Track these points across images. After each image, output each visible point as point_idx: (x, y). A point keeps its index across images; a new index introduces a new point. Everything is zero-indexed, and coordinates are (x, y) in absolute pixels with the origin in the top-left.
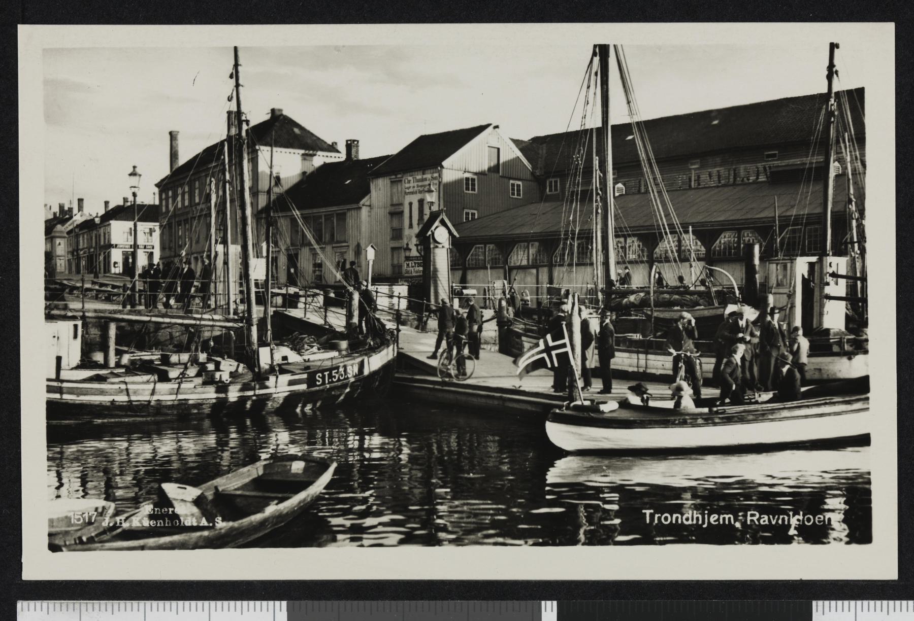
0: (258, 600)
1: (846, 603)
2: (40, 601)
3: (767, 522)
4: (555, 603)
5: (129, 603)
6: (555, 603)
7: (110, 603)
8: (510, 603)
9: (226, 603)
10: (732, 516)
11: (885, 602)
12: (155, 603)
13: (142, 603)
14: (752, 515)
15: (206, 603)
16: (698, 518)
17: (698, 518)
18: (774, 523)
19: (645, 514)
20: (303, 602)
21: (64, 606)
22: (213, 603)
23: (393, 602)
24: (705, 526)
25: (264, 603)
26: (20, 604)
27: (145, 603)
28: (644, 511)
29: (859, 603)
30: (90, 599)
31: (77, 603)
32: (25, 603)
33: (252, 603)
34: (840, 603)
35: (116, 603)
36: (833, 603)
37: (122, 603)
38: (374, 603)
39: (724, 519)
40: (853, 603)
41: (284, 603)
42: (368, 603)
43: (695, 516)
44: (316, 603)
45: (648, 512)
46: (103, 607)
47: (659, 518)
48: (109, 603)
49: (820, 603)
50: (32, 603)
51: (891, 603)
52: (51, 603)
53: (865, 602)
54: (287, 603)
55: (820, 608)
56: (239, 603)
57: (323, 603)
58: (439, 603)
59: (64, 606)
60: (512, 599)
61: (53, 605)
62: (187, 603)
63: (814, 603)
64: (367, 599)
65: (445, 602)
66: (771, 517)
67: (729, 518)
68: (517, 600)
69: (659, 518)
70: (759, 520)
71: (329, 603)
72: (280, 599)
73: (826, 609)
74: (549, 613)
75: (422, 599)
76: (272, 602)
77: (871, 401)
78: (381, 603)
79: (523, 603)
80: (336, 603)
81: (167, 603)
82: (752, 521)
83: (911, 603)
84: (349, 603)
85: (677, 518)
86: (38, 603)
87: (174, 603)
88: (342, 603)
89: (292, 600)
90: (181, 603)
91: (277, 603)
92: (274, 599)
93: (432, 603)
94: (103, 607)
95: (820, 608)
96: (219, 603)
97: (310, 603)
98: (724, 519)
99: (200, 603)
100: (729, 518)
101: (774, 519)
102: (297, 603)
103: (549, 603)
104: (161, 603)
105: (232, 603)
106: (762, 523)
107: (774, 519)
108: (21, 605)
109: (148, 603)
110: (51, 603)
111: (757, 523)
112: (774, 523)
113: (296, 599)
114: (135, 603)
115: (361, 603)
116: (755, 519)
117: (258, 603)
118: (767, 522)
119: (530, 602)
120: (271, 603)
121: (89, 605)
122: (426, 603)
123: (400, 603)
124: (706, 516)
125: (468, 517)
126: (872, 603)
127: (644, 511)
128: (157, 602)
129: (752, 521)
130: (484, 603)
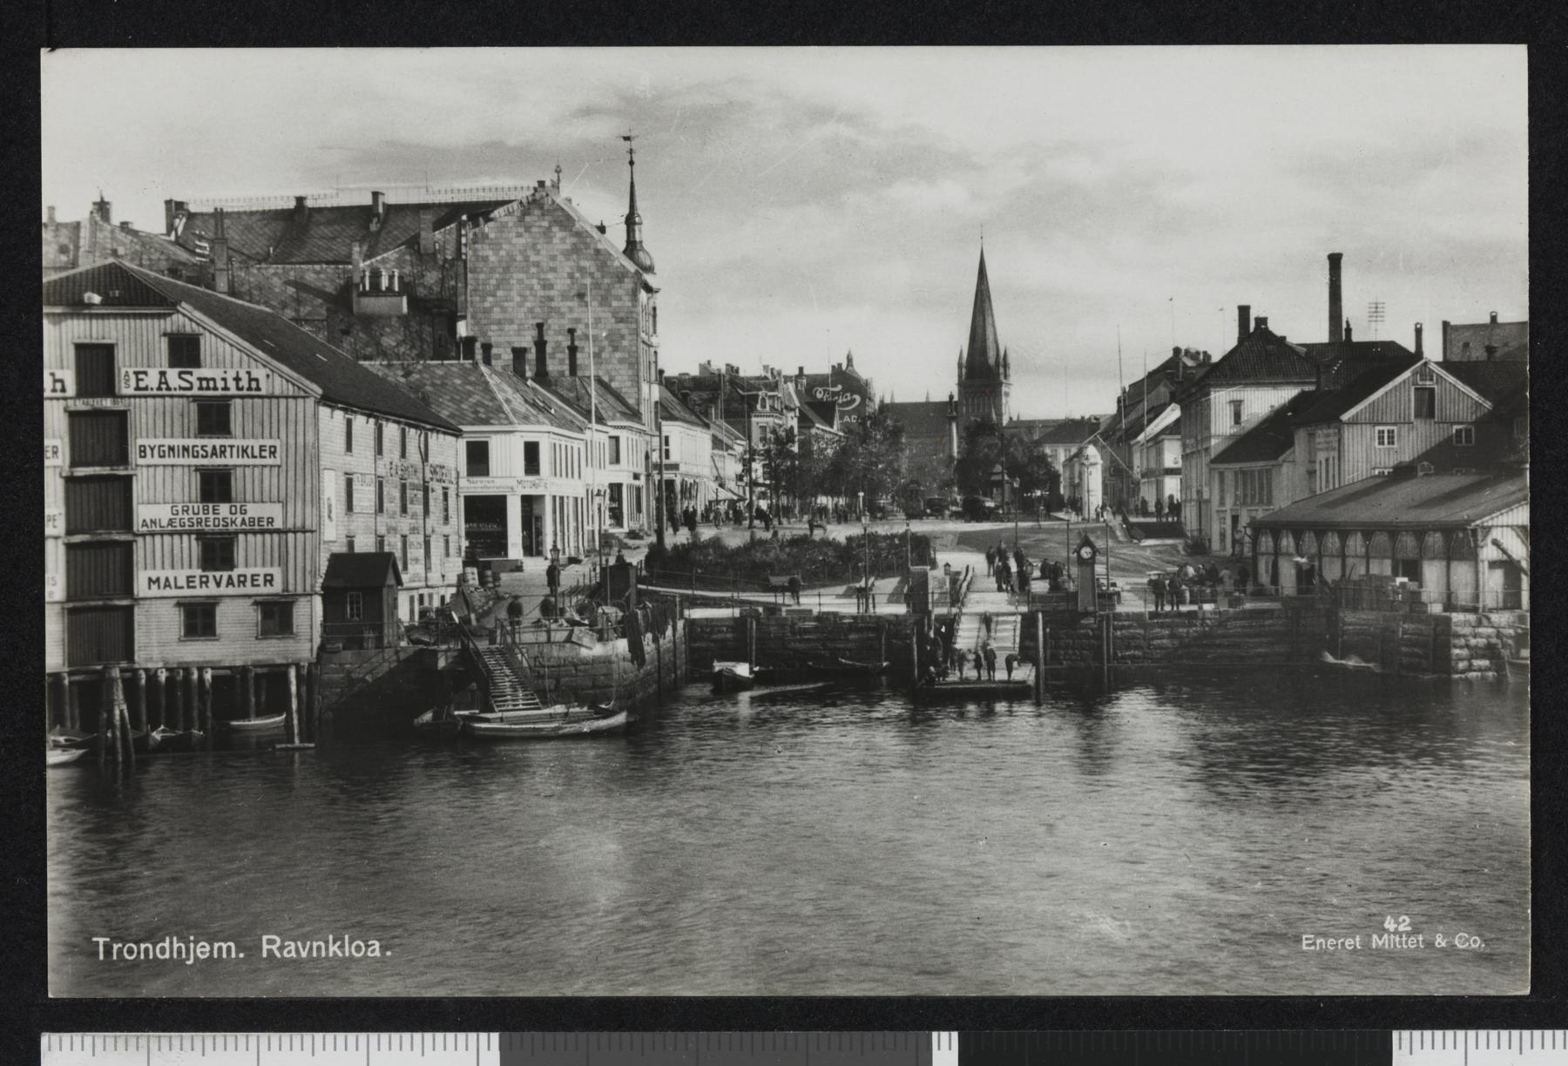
0: (450, 1031)
1: (1450, 1033)
2: (80, 1034)
3: (293, 954)
4: (955, 1035)
5: (230, 1036)
6: (955, 1035)
7: (198, 1036)
8: (878, 1035)
9: (395, 1036)
10: (232, 944)
11: (1515, 1033)
12: (275, 1036)
13: (253, 1036)
14: (271, 942)
15: (363, 1036)
16: (179, 952)
17: (179, 949)
18: (304, 954)
19: (98, 942)
20: (527, 1035)
21: (121, 1042)
22: (373, 1036)
23: (680, 1035)
24: (188, 963)
25: (461, 1036)
26: (46, 1039)
27: (182, 1037)
28: (95, 939)
29: (1471, 1033)
30: (164, 1031)
31: (143, 1037)
32: (55, 1037)
33: (439, 1036)
34: (1439, 1034)
35: (209, 1036)
36: (1428, 1034)
37: (220, 1036)
38: (648, 1035)
39: (220, 949)
40: (1461, 1034)
41: (495, 1036)
42: (637, 1035)
43: (176, 946)
44: (549, 1036)
45: (101, 940)
46: (187, 1043)
47: (120, 951)
48: (198, 1037)
49: (1406, 1034)
50: (66, 1037)
51: (1526, 1033)
52: (99, 1036)
53: (1482, 1033)
54: (500, 1037)
55: (1406, 1043)
56: (417, 1036)
57: (560, 1035)
58: (758, 1035)
59: (121, 1042)
60: (881, 1029)
61: (244, 1039)
62: (330, 1036)
63: (1395, 1034)
64: (636, 1030)
65: (769, 1034)
66: (299, 944)
67: (229, 949)
68: (891, 1029)
69: (120, 951)
70: (281, 949)
71: (571, 1035)
72: (488, 1028)
73: (1416, 1045)
74: (945, 1052)
75: (729, 1029)
76: (475, 1034)
77: (565, 495)
78: (658, 1035)
79: (901, 1035)
80: (583, 1035)
81: (297, 1036)
82: (270, 952)
83: (1559, 1033)
84: (604, 1035)
85: (147, 950)
86: (77, 1037)
87: (308, 1036)
88: (593, 1035)
89: (509, 1030)
90: (319, 1036)
91: (483, 1036)
92: (477, 1030)
93: (747, 1035)
94: (187, 1043)
95: (1406, 1043)
96: (384, 1036)
97: (538, 1035)
98: (220, 949)
99: (352, 1036)
100: (229, 949)
101: (304, 948)
102: (516, 1035)
103: (944, 1035)
104: (286, 1036)
105: (406, 1036)
106: (286, 955)
107: (304, 948)
108: (46, 1039)
109: (264, 1036)
110: (99, 1037)
111: (278, 955)
112: (304, 954)
113: (515, 1030)
114: (241, 1036)
115: (626, 1035)
116: (274, 947)
117: (450, 1036)
118: (293, 954)
119: (912, 1034)
120: (472, 1036)
121: (163, 1040)
122: (736, 1035)
123: (692, 1035)
124: (192, 945)
125: (1254, 736)
126: (1493, 1033)
127: (95, 939)
128: (278, 1034)
129: (270, 952)
130: (835, 1035)
